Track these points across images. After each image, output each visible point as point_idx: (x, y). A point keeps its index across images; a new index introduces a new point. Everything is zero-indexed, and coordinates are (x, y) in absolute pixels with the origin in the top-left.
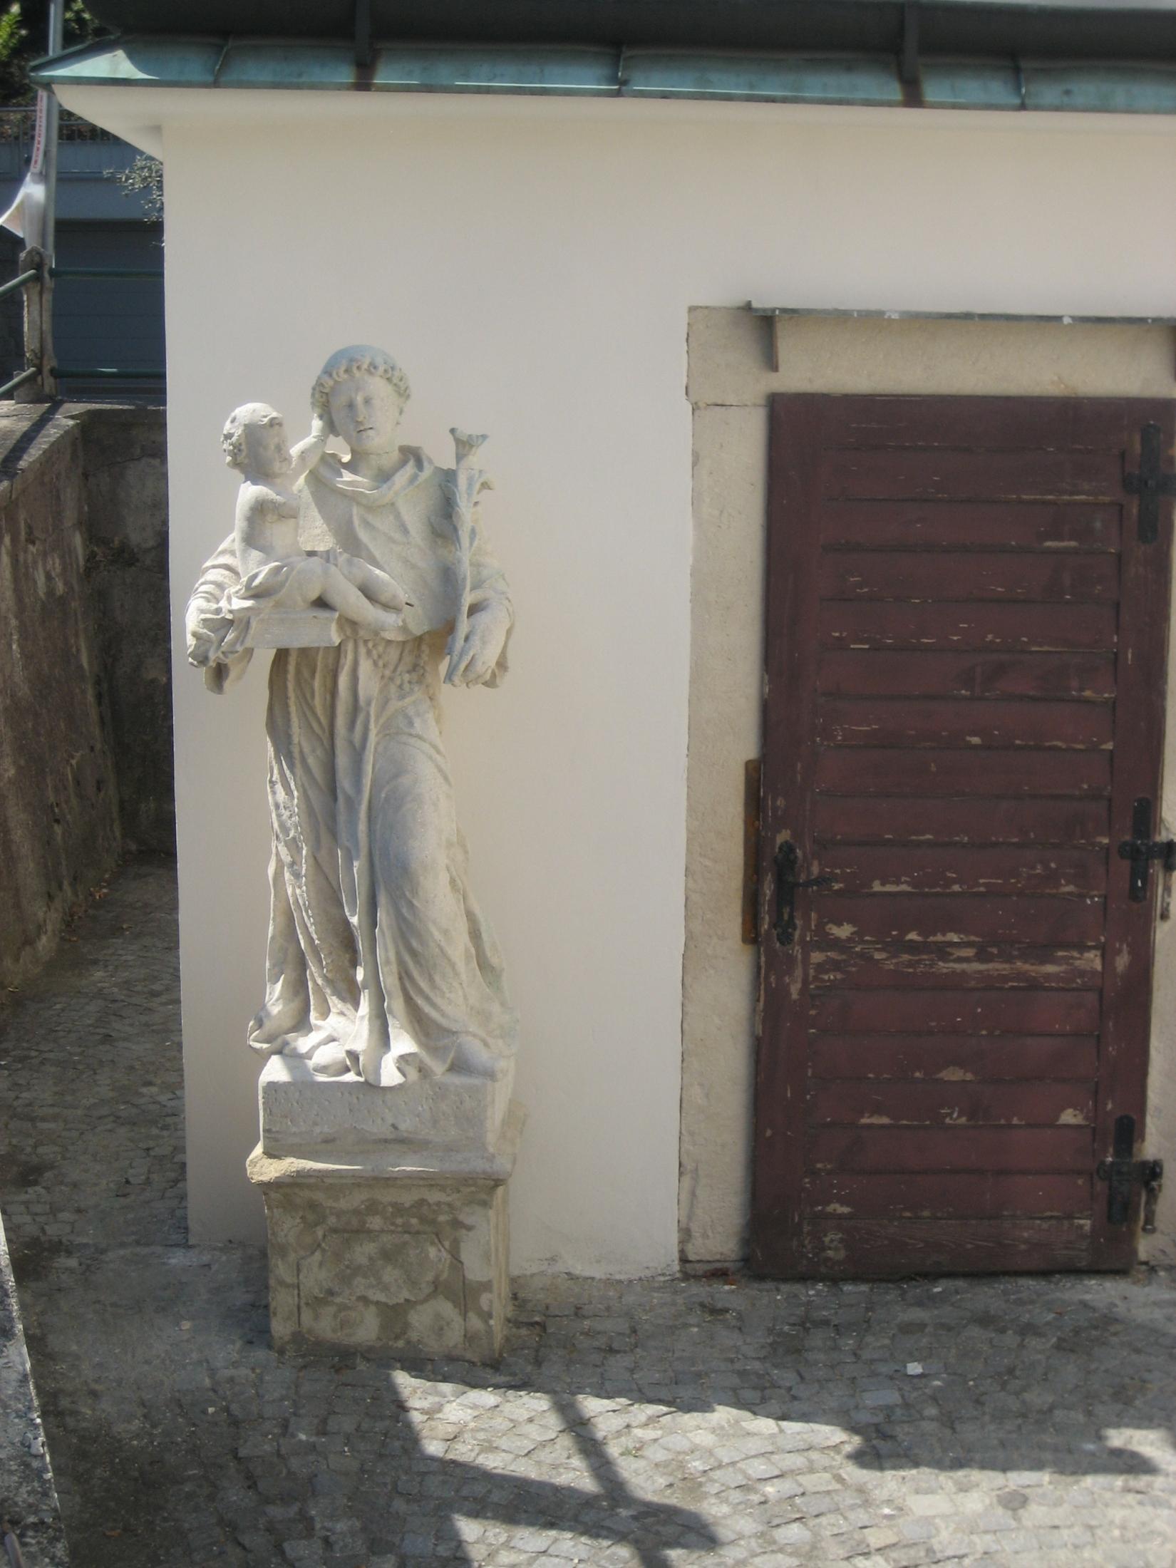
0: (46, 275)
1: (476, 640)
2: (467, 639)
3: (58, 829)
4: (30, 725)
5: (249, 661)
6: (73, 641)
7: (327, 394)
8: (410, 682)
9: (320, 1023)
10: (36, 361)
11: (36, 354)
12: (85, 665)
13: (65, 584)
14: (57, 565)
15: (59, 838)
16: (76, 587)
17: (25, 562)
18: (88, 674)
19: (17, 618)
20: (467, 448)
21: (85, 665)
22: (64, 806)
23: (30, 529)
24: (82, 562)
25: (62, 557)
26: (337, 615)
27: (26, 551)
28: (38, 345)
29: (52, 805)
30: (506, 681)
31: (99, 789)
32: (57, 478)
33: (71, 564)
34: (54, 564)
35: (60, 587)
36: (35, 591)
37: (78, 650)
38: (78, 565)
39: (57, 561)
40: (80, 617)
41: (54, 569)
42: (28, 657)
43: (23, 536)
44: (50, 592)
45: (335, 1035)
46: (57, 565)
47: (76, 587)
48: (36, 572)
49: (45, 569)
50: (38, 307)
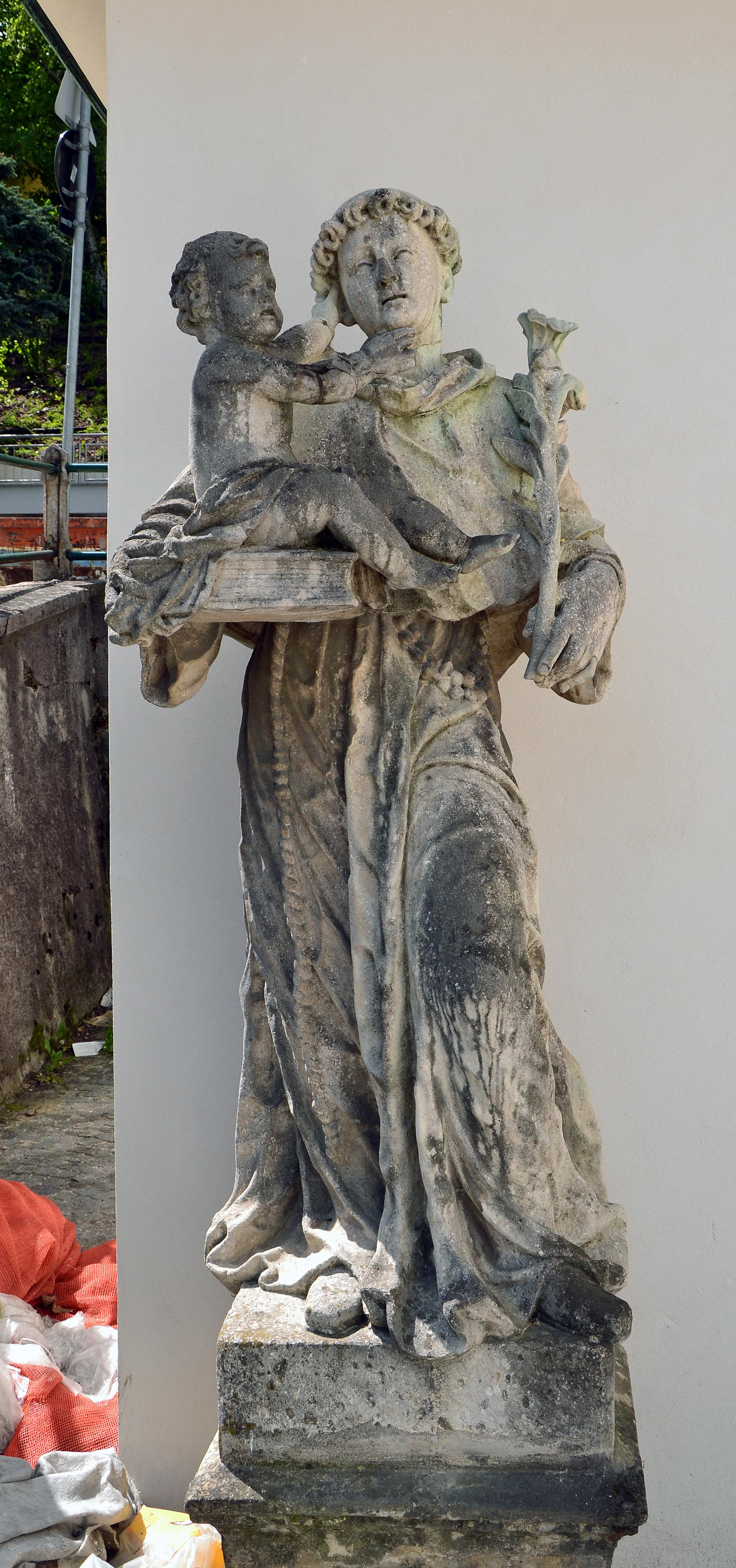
0: (64, 470)
1: (572, 612)
2: (559, 610)
3: (50, 960)
4: (22, 856)
5: (210, 663)
6: (75, 786)
7: (335, 253)
8: (463, 687)
9: (319, 1233)
10: (55, 545)
11: (53, 539)
12: (88, 808)
13: (69, 732)
14: (61, 713)
15: (51, 968)
16: (81, 738)
17: (25, 701)
18: (90, 818)
19: (11, 751)
20: (546, 338)
21: (88, 808)
22: (58, 937)
23: (30, 672)
24: (88, 718)
25: (67, 707)
26: (354, 557)
27: (25, 692)
28: (55, 530)
29: (45, 935)
30: (609, 687)
31: (97, 924)
32: (63, 635)
33: (76, 717)
34: (57, 711)
35: (63, 735)
36: (35, 731)
37: (81, 795)
38: (84, 719)
39: (61, 710)
40: (83, 766)
41: (57, 716)
42: (24, 792)
43: (22, 678)
44: (52, 736)
45: (344, 1257)
46: (61, 713)
47: (81, 738)
48: (36, 714)
49: (47, 715)
50: (56, 498)
